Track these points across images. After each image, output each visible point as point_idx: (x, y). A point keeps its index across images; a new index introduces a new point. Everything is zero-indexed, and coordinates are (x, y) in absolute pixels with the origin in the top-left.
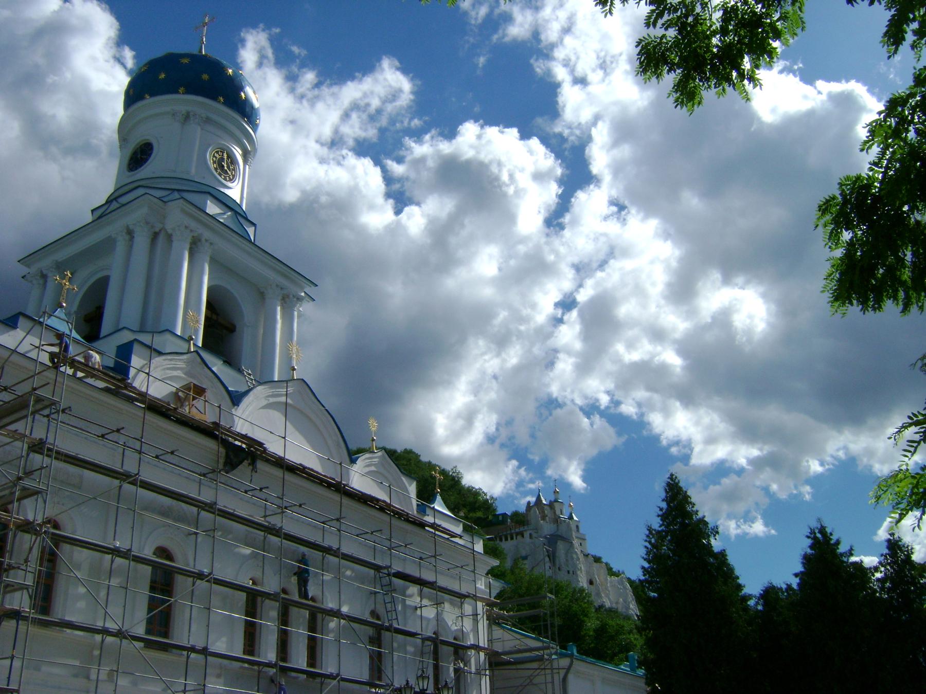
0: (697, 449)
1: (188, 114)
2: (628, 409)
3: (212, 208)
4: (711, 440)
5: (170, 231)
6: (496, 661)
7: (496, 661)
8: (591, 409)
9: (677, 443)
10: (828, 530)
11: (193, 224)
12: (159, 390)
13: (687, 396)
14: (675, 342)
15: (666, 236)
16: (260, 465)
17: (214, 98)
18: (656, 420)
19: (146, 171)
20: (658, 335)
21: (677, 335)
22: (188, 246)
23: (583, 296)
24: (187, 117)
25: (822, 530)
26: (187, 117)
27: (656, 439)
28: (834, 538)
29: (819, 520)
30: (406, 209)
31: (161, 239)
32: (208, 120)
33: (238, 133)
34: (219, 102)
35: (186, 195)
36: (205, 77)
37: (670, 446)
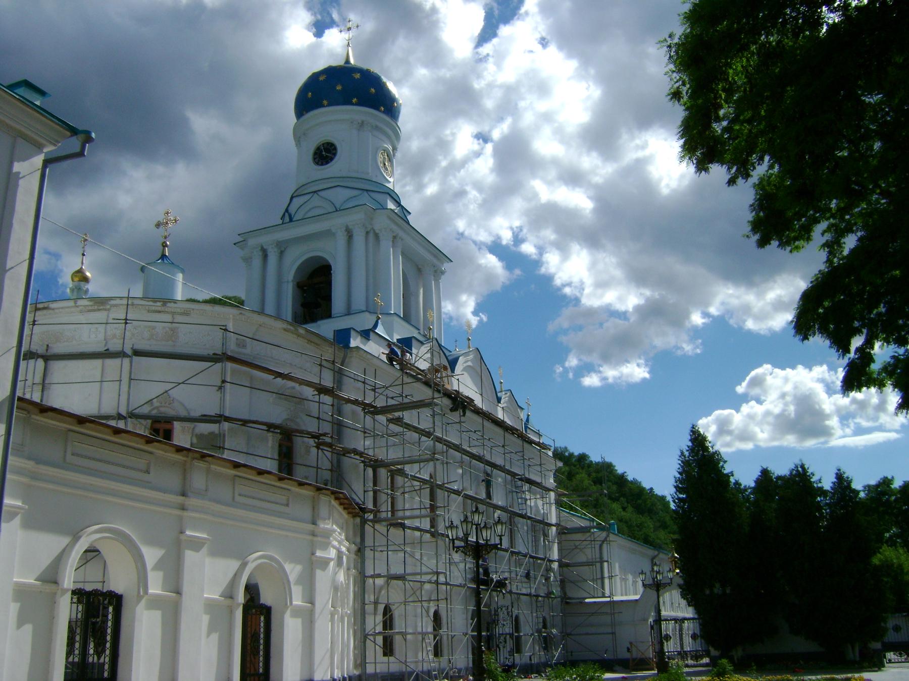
0: (587, 291)
1: (363, 122)
2: (528, 248)
3: (391, 205)
4: (602, 285)
5: (377, 231)
6: (563, 531)
7: (563, 531)
8: (496, 248)
9: (569, 284)
10: (806, 467)
11: (395, 228)
12: (423, 365)
13: (591, 238)
14: (597, 187)
15: (868, 388)
16: (468, 413)
17: (377, 108)
18: (552, 260)
19: (335, 168)
20: (573, 178)
21: (598, 179)
22: (391, 243)
23: (496, 134)
24: (362, 125)
25: (802, 466)
26: (362, 125)
27: (549, 278)
28: (810, 471)
29: (801, 460)
30: (327, 32)
31: (371, 235)
32: (377, 128)
33: (390, 133)
34: (380, 111)
35: (372, 194)
36: (373, 90)
37: (564, 286)
